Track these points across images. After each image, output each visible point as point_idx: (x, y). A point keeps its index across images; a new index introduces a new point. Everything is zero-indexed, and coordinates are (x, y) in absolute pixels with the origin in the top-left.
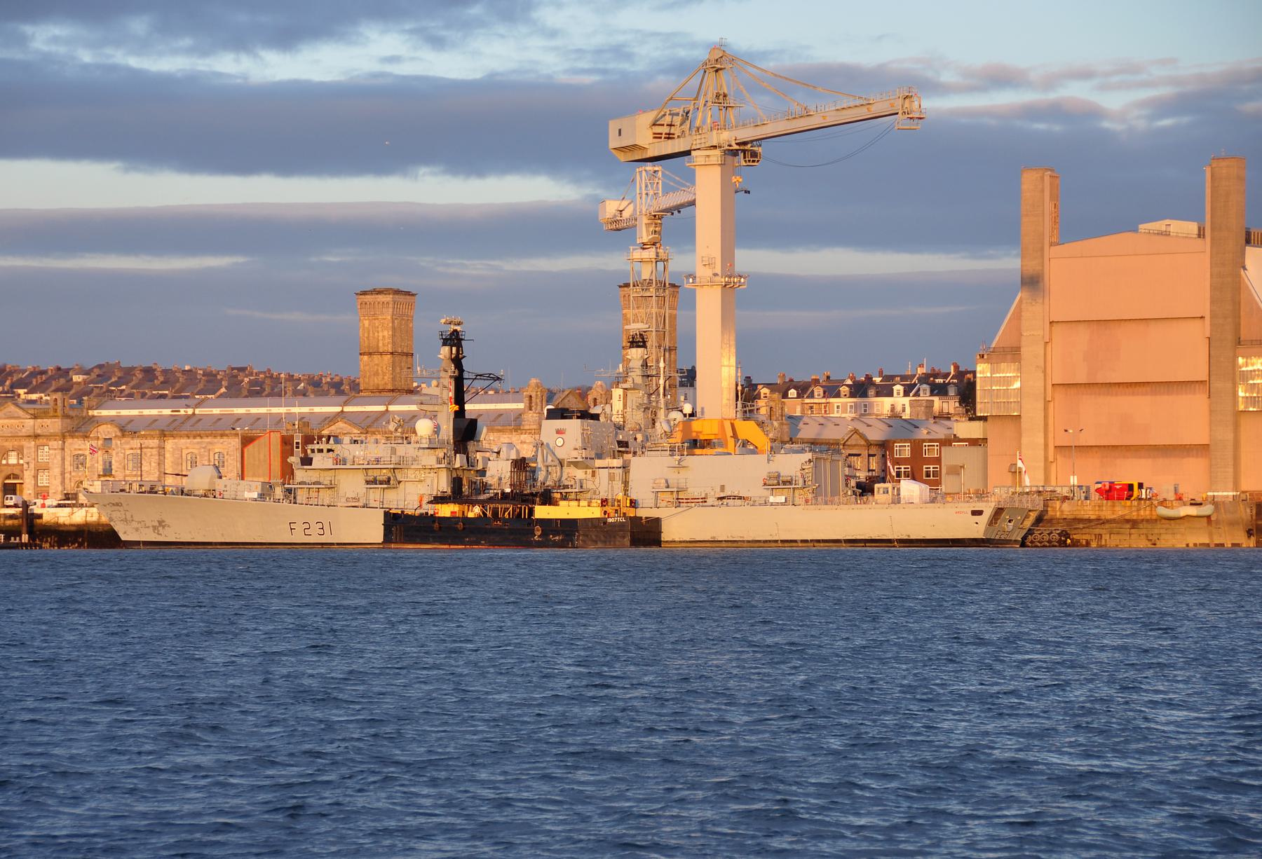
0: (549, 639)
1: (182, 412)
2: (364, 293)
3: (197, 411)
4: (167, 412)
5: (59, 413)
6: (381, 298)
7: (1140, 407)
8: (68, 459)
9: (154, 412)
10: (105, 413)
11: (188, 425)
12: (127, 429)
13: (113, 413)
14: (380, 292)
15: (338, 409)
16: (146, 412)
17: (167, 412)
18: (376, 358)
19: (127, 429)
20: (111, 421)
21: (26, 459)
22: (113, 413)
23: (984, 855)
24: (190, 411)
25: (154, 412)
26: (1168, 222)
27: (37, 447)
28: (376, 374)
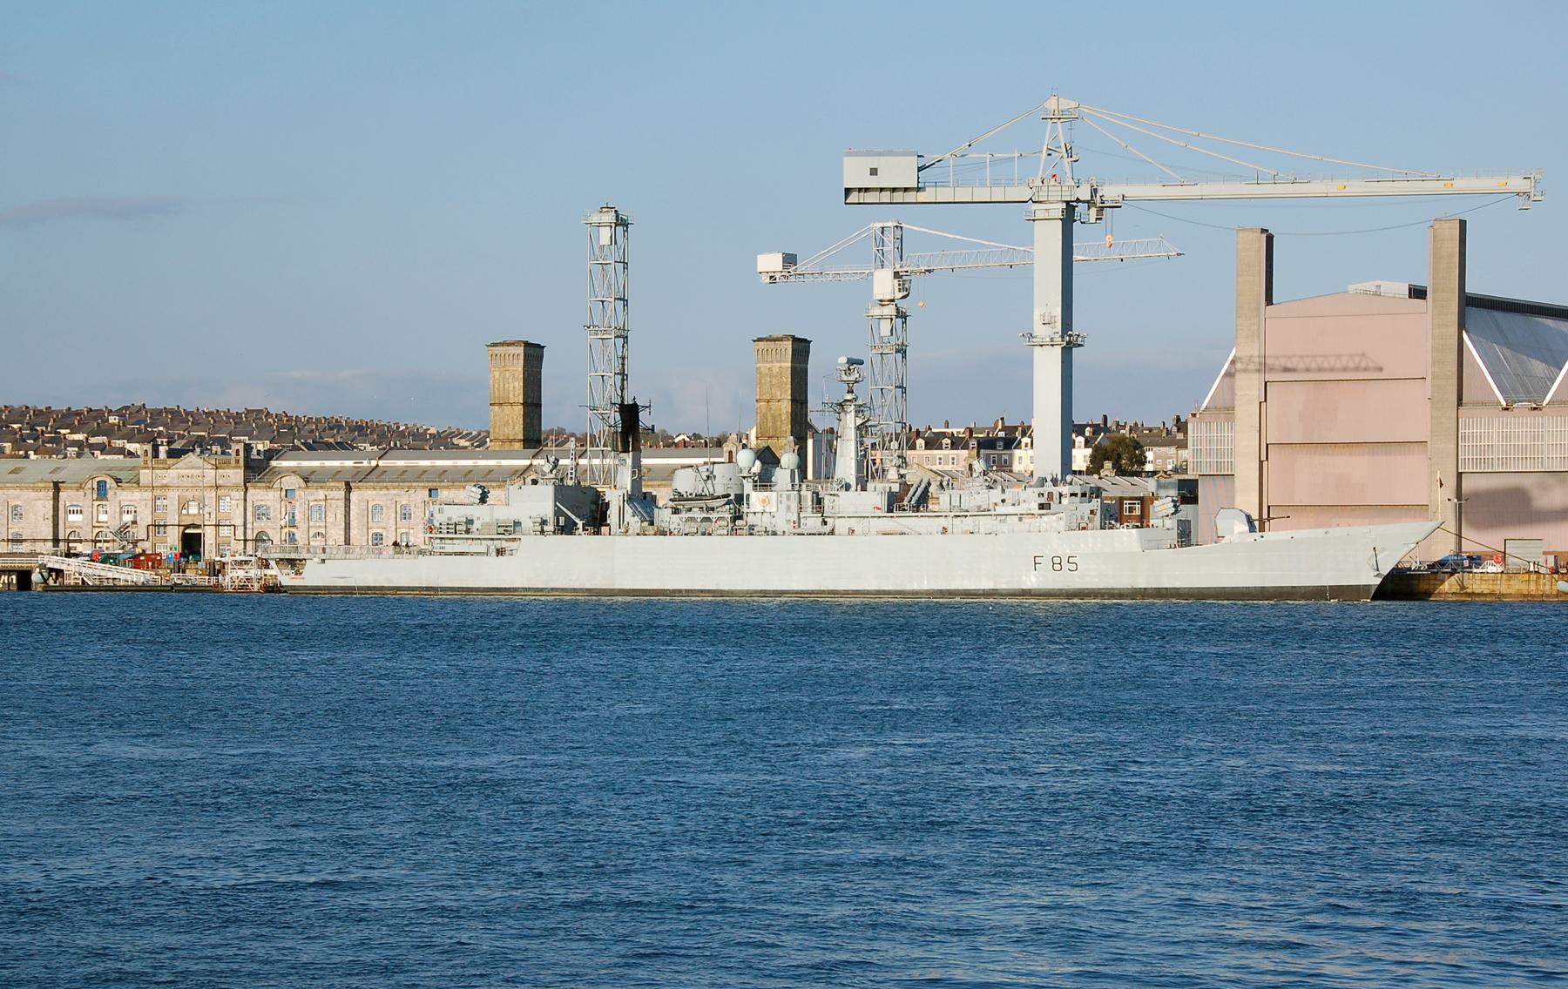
0: (1229, 661)
1: (365, 463)
2: (495, 345)
3: (381, 463)
4: (349, 463)
5: (242, 463)
6: (512, 350)
7: (1357, 466)
8: (250, 509)
9: (336, 463)
10: (285, 464)
11: (372, 476)
12: (307, 478)
13: (293, 464)
14: (509, 345)
15: (527, 462)
16: (328, 463)
17: (349, 463)
18: (507, 409)
19: (307, 478)
20: (294, 471)
21: (207, 509)
22: (293, 464)
23: (770, 983)
24: (374, 463)
25: (336, 463)
26: (1378, 283)
27: (219, 498)
28: (507, 424)
